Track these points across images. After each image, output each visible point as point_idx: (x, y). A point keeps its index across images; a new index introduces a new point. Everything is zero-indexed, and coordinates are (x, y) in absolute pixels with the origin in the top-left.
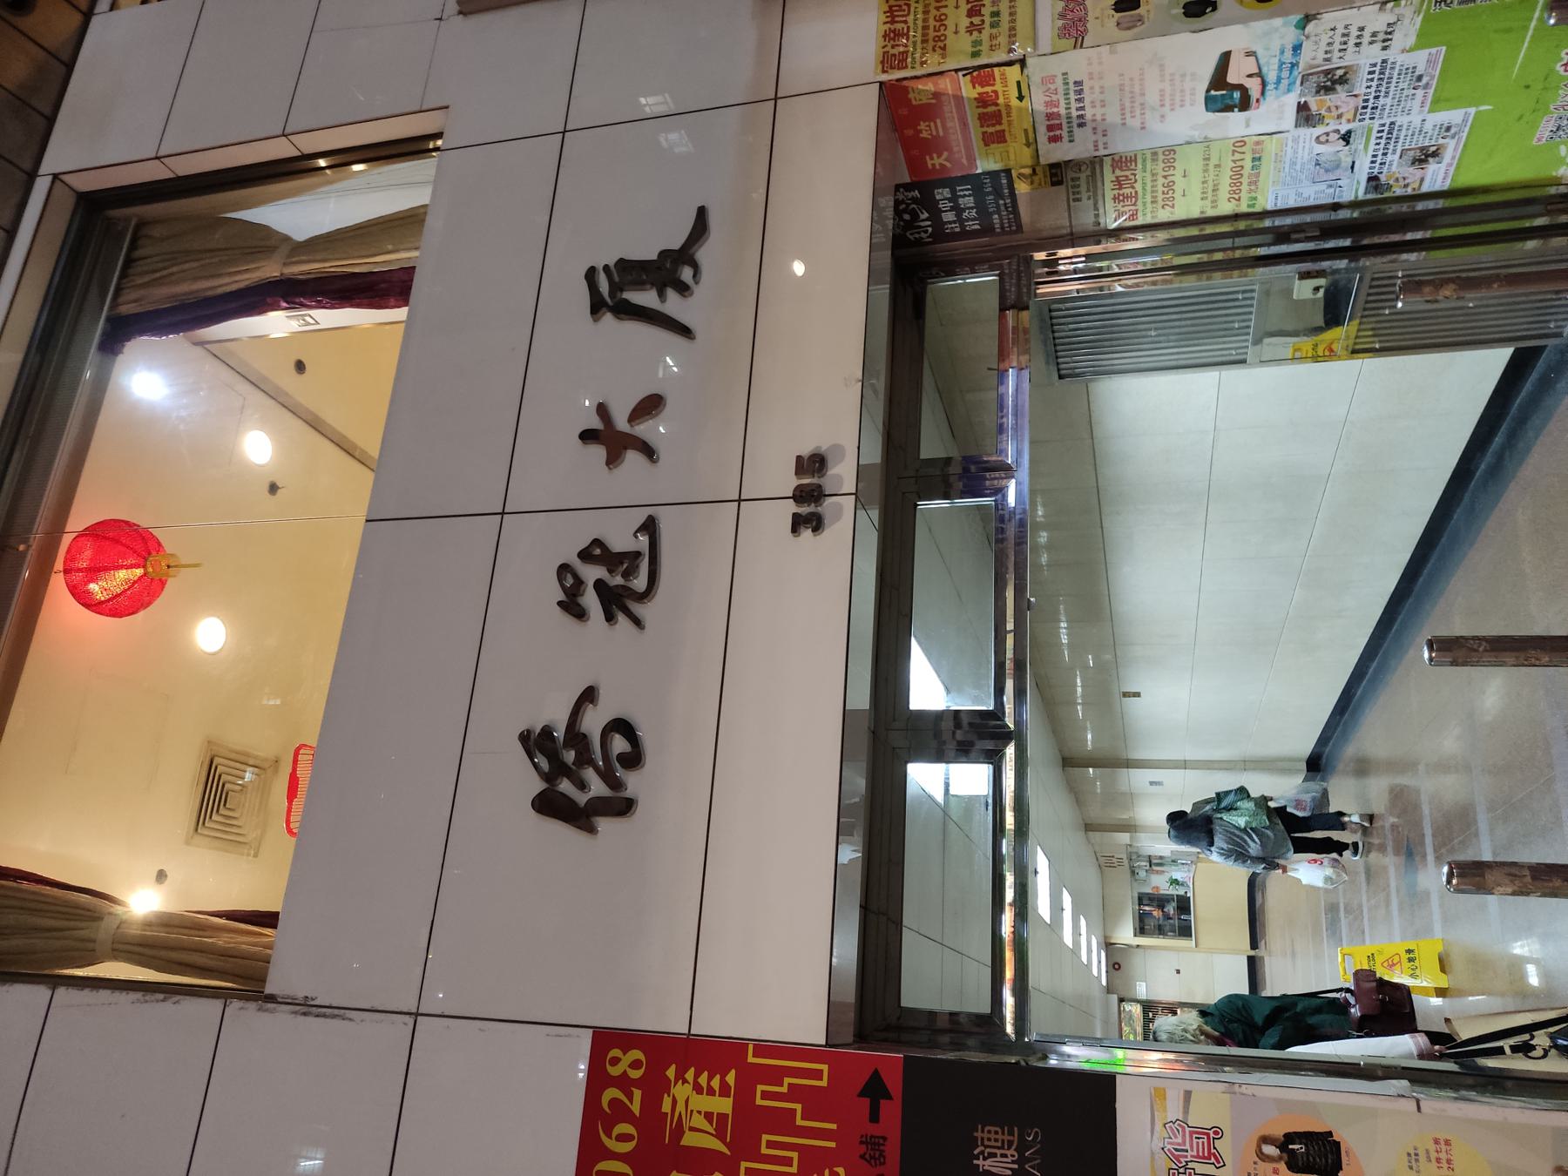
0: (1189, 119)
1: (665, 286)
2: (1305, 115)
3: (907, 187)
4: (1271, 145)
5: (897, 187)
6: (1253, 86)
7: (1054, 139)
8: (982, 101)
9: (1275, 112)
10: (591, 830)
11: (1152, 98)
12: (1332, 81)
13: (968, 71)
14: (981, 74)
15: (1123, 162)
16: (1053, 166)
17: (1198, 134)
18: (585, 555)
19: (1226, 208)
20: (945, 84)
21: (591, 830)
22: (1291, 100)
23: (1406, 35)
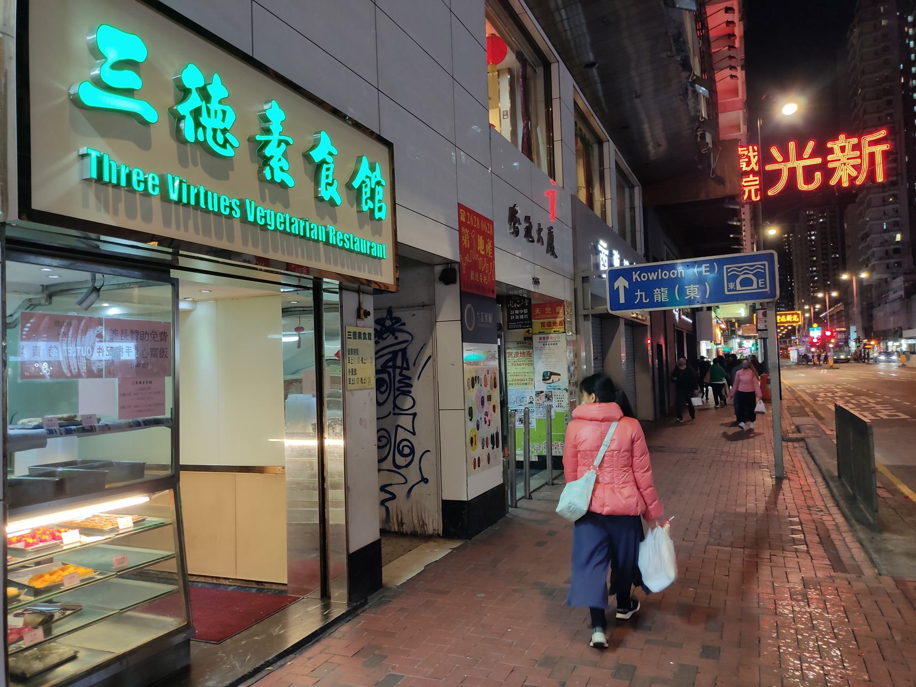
0: (541, 367)
1: (265, 157)
2: (539, 393)
3: (530, 303)
4: (531, 387)
5: (530, 299)
6: (550, 381)
7: (540, 338)
8: (555, 323)
9: (542, 386)
10: (282, 180)
11: (549, 360)
12: (548, 397)
13: (564, 321)
14: (563, 323)
15: (530, 355)
16: (531, 338)
17: (714, 411)
18: (533, 241)
19: (509, 378)
20: (561, 315)
21: (282, 180)
22: (544, 389)
23: (559, 410)
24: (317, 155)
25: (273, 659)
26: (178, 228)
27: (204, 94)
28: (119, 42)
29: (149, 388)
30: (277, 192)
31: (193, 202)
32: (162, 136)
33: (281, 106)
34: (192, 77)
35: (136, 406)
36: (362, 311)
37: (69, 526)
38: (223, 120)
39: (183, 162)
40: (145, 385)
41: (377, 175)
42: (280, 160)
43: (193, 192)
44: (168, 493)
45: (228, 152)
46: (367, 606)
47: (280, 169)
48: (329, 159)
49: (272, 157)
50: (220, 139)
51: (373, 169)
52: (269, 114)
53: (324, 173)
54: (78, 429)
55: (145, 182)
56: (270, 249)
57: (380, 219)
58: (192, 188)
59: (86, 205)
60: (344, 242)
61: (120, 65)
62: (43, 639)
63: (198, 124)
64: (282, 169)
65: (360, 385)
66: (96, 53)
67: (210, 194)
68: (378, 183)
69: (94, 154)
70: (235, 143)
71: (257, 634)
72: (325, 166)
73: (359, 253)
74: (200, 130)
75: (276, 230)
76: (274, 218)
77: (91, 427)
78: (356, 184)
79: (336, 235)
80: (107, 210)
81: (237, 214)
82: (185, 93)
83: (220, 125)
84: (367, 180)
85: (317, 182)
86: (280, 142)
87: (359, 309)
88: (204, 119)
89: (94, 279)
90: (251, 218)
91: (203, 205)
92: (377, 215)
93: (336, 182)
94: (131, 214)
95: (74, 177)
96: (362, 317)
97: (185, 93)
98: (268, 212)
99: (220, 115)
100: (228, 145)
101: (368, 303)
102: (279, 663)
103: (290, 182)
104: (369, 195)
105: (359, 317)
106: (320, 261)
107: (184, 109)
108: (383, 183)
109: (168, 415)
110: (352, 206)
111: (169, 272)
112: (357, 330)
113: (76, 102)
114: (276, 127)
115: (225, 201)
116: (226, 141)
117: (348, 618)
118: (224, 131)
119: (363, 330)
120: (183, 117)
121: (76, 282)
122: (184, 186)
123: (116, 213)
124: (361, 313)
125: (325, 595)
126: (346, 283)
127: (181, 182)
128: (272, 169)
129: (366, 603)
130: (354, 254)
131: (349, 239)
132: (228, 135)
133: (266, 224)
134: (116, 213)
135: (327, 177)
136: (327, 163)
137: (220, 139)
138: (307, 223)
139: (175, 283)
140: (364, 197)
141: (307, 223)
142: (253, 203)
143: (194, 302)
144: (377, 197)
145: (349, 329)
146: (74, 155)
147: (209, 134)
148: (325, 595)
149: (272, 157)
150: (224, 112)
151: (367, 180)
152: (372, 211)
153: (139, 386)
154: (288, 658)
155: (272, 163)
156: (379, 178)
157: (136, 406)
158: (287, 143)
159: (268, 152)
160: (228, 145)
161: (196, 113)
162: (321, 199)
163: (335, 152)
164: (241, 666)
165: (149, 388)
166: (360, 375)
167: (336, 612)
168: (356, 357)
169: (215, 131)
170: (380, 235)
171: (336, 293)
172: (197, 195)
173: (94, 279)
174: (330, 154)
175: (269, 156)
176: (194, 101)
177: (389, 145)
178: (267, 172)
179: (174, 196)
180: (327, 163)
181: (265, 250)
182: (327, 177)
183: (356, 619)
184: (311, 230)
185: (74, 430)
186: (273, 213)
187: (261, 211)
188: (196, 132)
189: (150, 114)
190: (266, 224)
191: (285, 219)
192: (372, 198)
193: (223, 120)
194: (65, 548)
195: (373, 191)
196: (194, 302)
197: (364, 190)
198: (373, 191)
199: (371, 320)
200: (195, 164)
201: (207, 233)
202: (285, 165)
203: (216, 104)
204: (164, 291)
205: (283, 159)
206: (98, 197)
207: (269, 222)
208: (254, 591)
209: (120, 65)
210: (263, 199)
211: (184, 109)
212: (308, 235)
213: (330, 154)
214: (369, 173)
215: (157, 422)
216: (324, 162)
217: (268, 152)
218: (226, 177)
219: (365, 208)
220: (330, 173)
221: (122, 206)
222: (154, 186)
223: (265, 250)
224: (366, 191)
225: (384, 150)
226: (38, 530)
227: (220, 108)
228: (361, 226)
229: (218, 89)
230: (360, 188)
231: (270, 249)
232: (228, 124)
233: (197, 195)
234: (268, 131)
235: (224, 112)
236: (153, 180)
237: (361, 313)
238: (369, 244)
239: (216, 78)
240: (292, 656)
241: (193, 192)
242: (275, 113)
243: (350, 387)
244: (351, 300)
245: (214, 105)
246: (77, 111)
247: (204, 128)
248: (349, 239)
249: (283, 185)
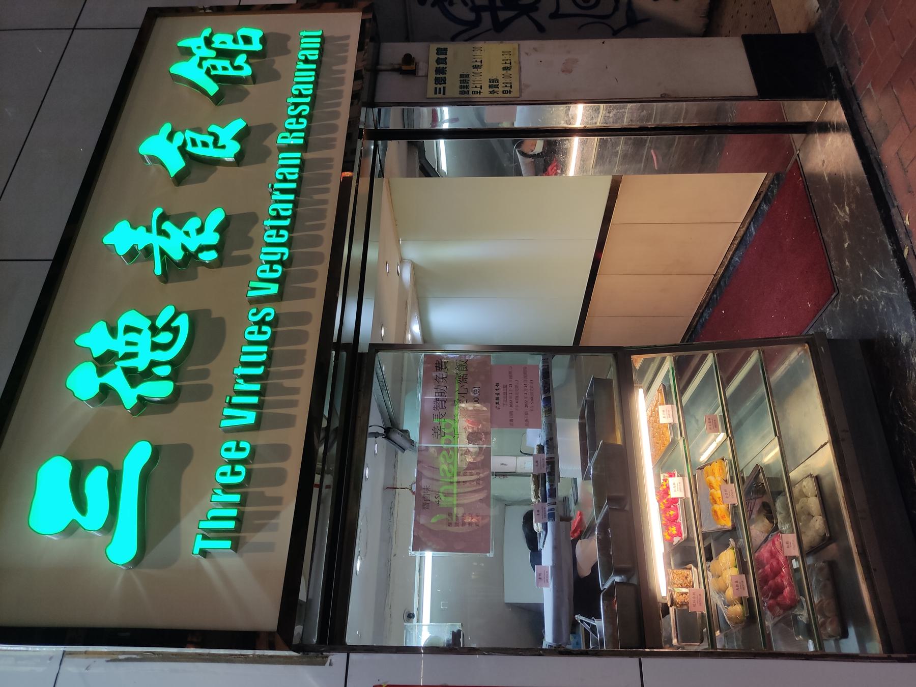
10: (216, 230)
21: (216, 230)
24: (175, 164)
25: (892, 243)
26: (293, 404)
27: (104, 362)
28: (49, 503)
29: (505, 386)
30: (236, 236)
31: (256, 387)
32: (172, 428)
33: (109, 228)
34: (83, 382)
35: (526, 406)
36: (404, 68)
37: (663, 493)
38: (139, 331)
39: (204, 393)
40: (501, 392)
41: (195, 43)
42: (187, 233)
43: (242, 386)
44: (638, 361)
45: (183, 322)
46: (842, 70)
47: (198, 235)
48: (179, 138)
49: (184, 248)
50: (164, 337)
51: (187, 53)
52: (122, 250)
53: (199, 151)
54: (550, 481)
55: (233, 462)
56: (322, 222)
57: (263, 40)
58: (237, 387)
59: (269, 547)
60: (299, 116)
61: (80, 502)
62: (795, 535)
63: (148, 374)
64: (200, 230)
65: (514, 72)
66: (72, 529)
67: (244, 358)
68: (208, 42)
69: (200, 544)
70: (167, 313)
71: (839, 241)
72: (190, 148)
73: (316, 83)
74: (158, 371)
75: (288, 244)
76: (272, 247)
77: (548, 463)
78: (212, 88)
79: (291, 131)
80: (275, 514)
81: (269, 311)
82: (106, 392)
83: (144, 340)
84: (206, 64)
85: (215, 162)
86: (162, 233)
87: (399, 71)
88: (141, 364)
89: (376, 435)
90: (274, 289)
91: (259, 371)
92: (256, 46)
93: (213, 128)
94: (279, 477)
95: (234, 564)
96: (413, 67)
97: (106, 392)
98: (263, 258)
99: (132, 337)
100: (173, 325)
101: (393, 52)
102: (902, 236)
103: (217, 216)
104: (227, 63)
105: (413, 73)
106: (331, 160)
107: (129, 396)
108: (207, 32)
109: (537, 361)
110: (247, 93)
111: (362, 354)
112: (432, 75)
113: (137, 561)
114: (141, 238)
115: (251, 333)
116: (167, 327)
117: (855, 107)
118: (154, 330)
119: (433, 65)
120: (141, 398)
121: (382, 416)
122: (236, 400)
123: (278, 501)
124: (408, 67)
125: (806, 128)
126: (364, 97)
127: (232, 405)
128: (202, 249)
129: (835, 70)
130: (319, 93)
131: (297, 105)
132: (160, 323)
133: (280, 262)
134: (278, 501)
135: (205, 144)
136: (185, 143)
137: (164, 337)
138: (277, 186)
139: (376, 348)
140: (231, 72)
141: (277, 186)
142: (252, 284)
143: (402, 261)
144: (230, 46)
145: (431, 93)
146: (204, 562)
147: (160, 356)
148: (806, 128)
149: (184, 248)
150: (128, 329)
151: (206, 64)
152: (251, 55)
153: (501, 401)
154: (897, 219)
155: (193, 248)
156: (200, 41)
157: (526, 406)
158: (163, 218)
159: (177, 255)
160: (173, 325)
161: (134, 377)
162: (240, 158)
163: (167, 128)
164: (890, 289)
165: (505, 386)
166: (497, 72)
167: (836, 112)
168: (472, 78)
169: (155, 346)
170: (287, 38)
171: (379, 111)
172: (248, 379)
173: (376, 435)
174: (170, 137)
175: (182, 253)
176: (116, 378)
177: (153, 14)
178: (209, 256)
179: (250, 417)
180: (185, 143)
181: (318, 258)
182: (205, 144)
183: (861, 95)
184: (285, 180)
185: (551, 486)
186: (265, 250)
187: (264, 271)
188: (160, 378)
189: (138, 456)
190: (280, 262)
191: (272, 227)
192: (229, 55)
193: (139, 331)
194: (689, 496)
195: (222, 54)
196: (402, 261)
197: (220, 72)
198: (222, 54)
199: (415, 49)
200: (205, 374)
201: (299, 357)
202: (193, 224)
203: (112, 353)
204: (385, 363)
205: (185, 228)
206: (258, 529)
207: (277, 258)
208: (765, 207)
209: (80, 502)
210: (247, 260)
211: (129, 396)
212: (293, 186)
213: (170, 137)
214: (195, 60)
215: (547, 374)
216: (182, 149)
217: (177, 255)
218: (221, 322)
219: (247, 71)
220: (199, 138)
221: (270, 491)
222: (239, 449)
223: (318, 258)
224: (223, 67)
225: (164, 25)
226: (664, 536)
227: (122, 337)
228: (275, 76)
229: (96, 339)
230: (217, 79)
231: (322, 222)
232: (144, 323)
233: (248, 379)
234: (148, 250)
235: (128, 329)
236: (229, 450)
237: (408, 67)
238: (301, 65)
239: (82, 340)
240: (894, 211)
241: (242, 386)
242: (122, 237)
243: (515, 93)
244: (390, 85)
245: (119, 345)
246: (149, 557)
247: (154, 364)
248: (297, 105)
249: (222, 229)
